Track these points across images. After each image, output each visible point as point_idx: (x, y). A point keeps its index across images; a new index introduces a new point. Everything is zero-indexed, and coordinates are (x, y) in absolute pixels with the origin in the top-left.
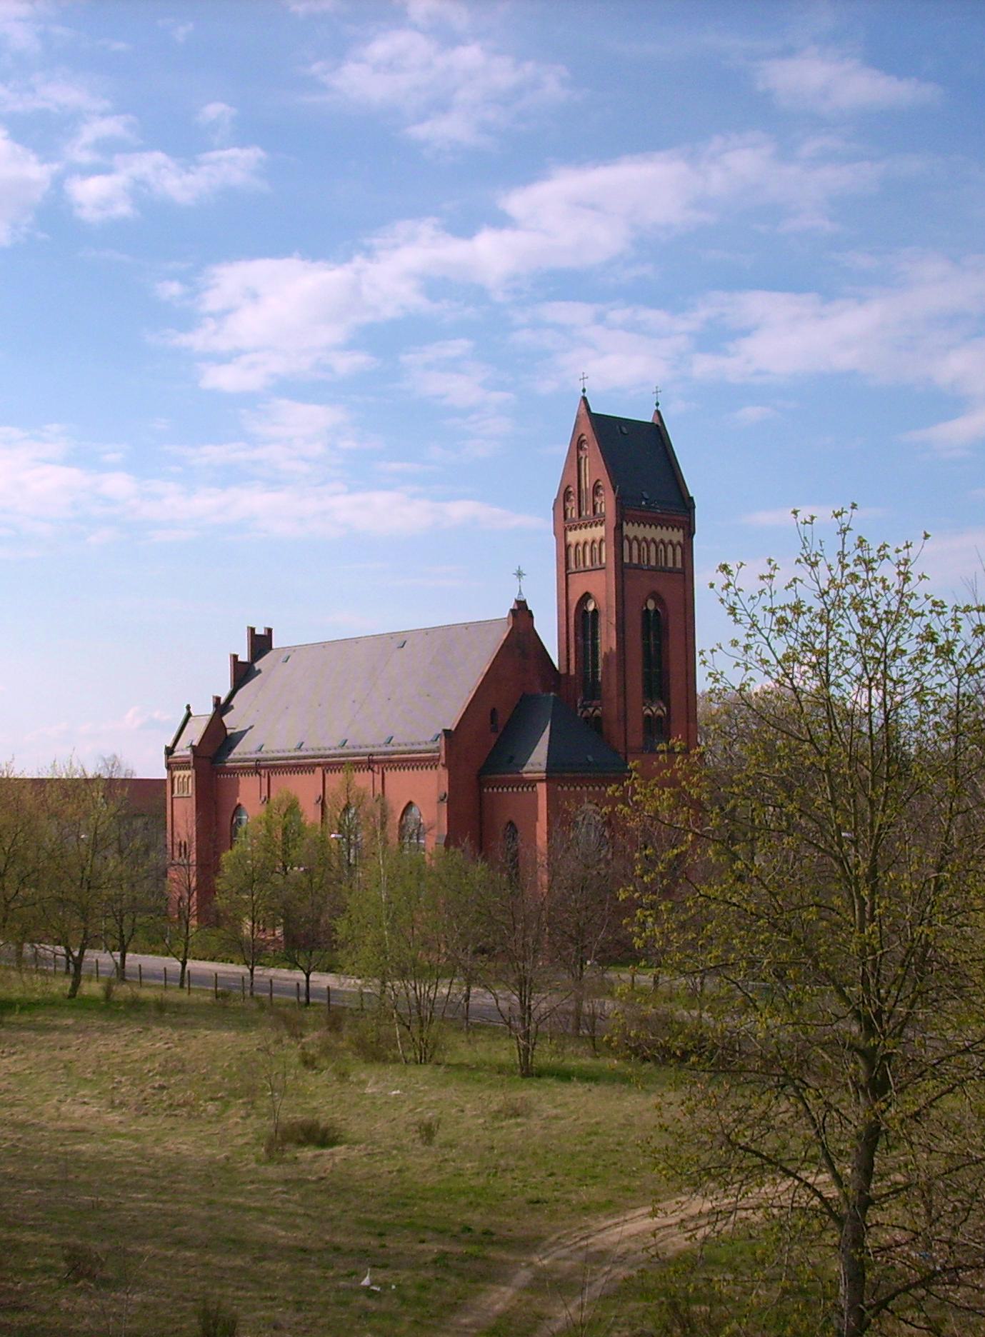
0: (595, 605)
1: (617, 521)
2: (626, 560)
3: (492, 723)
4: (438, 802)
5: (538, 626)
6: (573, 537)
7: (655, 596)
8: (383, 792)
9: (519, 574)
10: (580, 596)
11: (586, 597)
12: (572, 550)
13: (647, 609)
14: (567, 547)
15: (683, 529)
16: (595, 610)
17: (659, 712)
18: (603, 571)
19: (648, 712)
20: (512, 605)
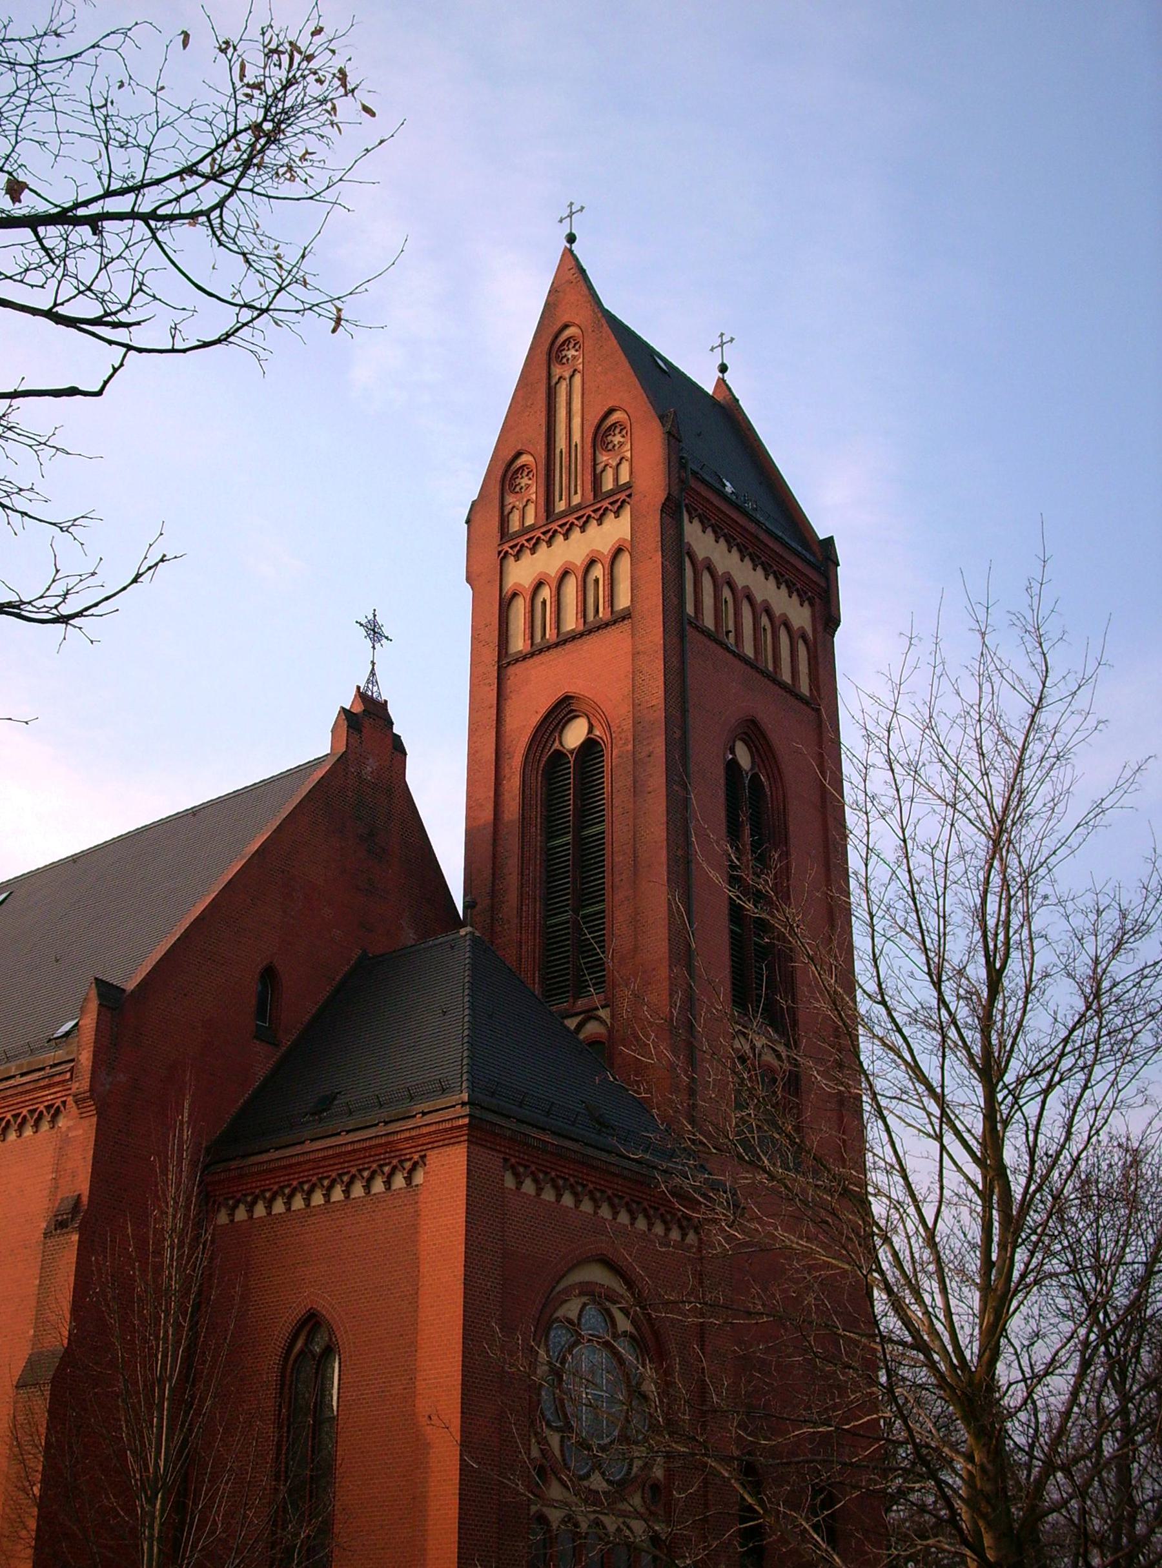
0: (590, 730)
2: (690, 609)
3: (261, 1012)
4: (47, 1235)
5: (414, 777)
6: (521, 573)
9: (374, 632)
10: (543, 711)
15: (812, 605)
16: (590, 746)
20: (347, 700)
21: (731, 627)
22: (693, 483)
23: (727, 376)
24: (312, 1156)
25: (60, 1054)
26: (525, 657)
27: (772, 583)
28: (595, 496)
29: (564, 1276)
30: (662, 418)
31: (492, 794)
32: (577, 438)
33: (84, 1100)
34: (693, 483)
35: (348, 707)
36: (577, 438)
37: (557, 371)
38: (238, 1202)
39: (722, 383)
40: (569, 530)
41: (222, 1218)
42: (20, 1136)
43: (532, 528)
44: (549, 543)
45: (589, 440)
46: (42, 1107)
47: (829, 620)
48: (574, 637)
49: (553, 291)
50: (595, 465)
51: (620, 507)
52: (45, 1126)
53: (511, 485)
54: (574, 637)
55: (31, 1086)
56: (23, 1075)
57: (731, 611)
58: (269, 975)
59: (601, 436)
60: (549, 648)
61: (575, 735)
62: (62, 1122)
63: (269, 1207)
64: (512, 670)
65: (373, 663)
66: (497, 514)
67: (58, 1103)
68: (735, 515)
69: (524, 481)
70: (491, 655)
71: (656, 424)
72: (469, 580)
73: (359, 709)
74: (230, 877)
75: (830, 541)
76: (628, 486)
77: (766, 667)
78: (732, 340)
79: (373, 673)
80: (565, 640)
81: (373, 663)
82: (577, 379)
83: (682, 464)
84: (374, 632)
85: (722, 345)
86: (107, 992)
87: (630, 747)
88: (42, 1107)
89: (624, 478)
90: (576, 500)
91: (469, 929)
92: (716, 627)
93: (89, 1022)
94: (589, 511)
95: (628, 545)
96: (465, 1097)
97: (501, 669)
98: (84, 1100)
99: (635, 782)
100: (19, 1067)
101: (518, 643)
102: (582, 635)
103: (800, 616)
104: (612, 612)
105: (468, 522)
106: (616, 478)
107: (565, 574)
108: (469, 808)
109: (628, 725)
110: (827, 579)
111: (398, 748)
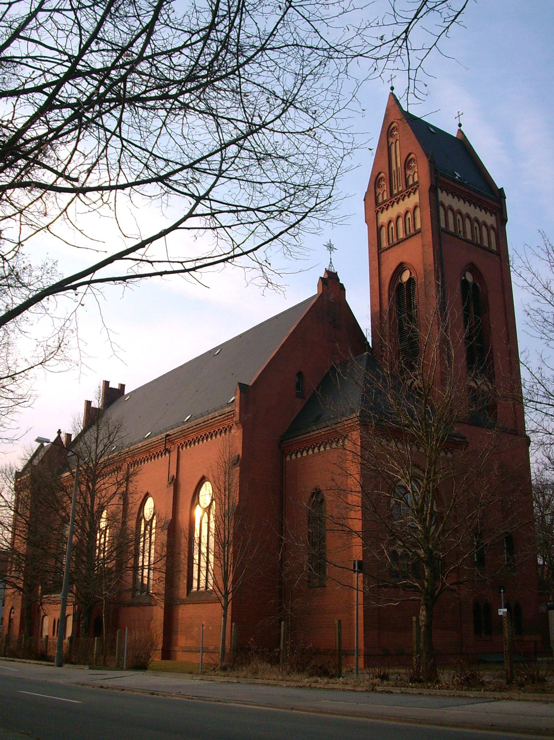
0: (411, 275)
1: (431, 181)
2: (443, 225)
6: (384, 218)
7: (472, 268)
8: (177, 473)
9: (330, 247)
10: (394, 268)
11: (400, 268)
12: (384, 231)
13: (465, 280)
14: (379, 230)
16: (411, 280)
17: (485, 388)
18: (419, 235)
19: (473, 384)
21: (461, 229)
22: (441, 178)
23: (462, 128)
24: (313, 436)
25: (230, 409)
26: (387, 249)
27: (478, 209)
28: (406, 187)
30: (427, 155)
31: (379, 300)
32: (399, 165)
33: (238, 423)
34: (441, 178)
35: (322, 276)
36: (399, 165)
37: (391, 140)
38: (292, 453)
39: (460, 131)
40: (398, 201)
41: (288, 459)
42: (216, 438)
43: (386, 201)
44: (392, 206)
45: (403, 166)
46: (226, 426)
47: (502, 219)
48: (403, 240)
49: (387, 109)
50: (405, 176)
51: (415, 191)
52: (227, 432)
53: (408, 166)
54: (403, 240)
55: (222, 420)
56: (220, 416)
57: (461, 223)
58: (300, 374)
59: (407, 164)
60: (394, 245)
61: (405, 277)
62: (233, 431)
63: (302, 454)
64: (383, 254)
65: (331, 259)
66: (374, 196)
67: (231, 425)
68: (459, 187)
69: (383, 183)
70: (375, 249)
71: (425, 158)
72: (366, 222)
73: (326, 277)
74: (283, 343)
75: (502, 189)
76: (417, 182)
77: (477, 242)
78: (462, 114)
79: (331, 263)
80: (400, 242)
81: (331, 259)
82: (398, 142)
83: (436, 171)
84: (330, 247)
85: (459, 116)
86: (243, 387)
87: (423, 280)
88: (226, 426)
89: (416, 180)
90: (400, 189)
91: (367, 353)
92: (455, 230)
93: (238, 397)
94: (404, 193)
95: (418, 204)
96: (358, 414)
97: (379, 255)
98: (238, 423)
99: (425, 293)
100: (218, 413)
101: (384, 244)
102: (405, 239)
103: (491, 220)
104: (397, 240)
105: (364, 200)
106: (413, 180)
107: (398, 217)
108: (371, 306)
109: (422, 272)
110: (501, 204)
111: (342, 288)
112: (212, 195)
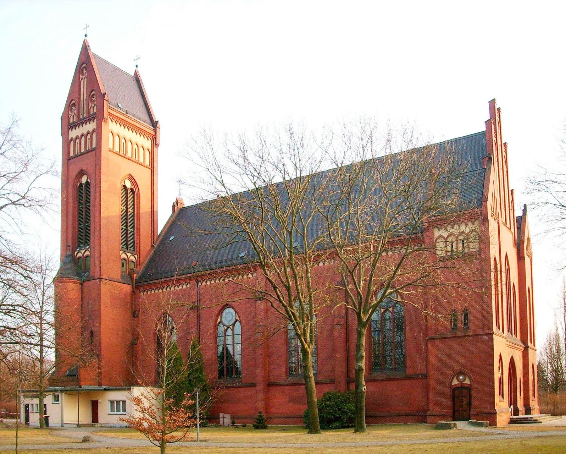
0: (87, 179)
6: (73, 134)
16: (87, 183)
29: (68, 137)
32: (85, 98)
36: (85, 98)
61: (84, 180)
72: (61, 118)
101: (72, 154)
106: (93, 111)
107: (82, 136)
112: (6, 154)
